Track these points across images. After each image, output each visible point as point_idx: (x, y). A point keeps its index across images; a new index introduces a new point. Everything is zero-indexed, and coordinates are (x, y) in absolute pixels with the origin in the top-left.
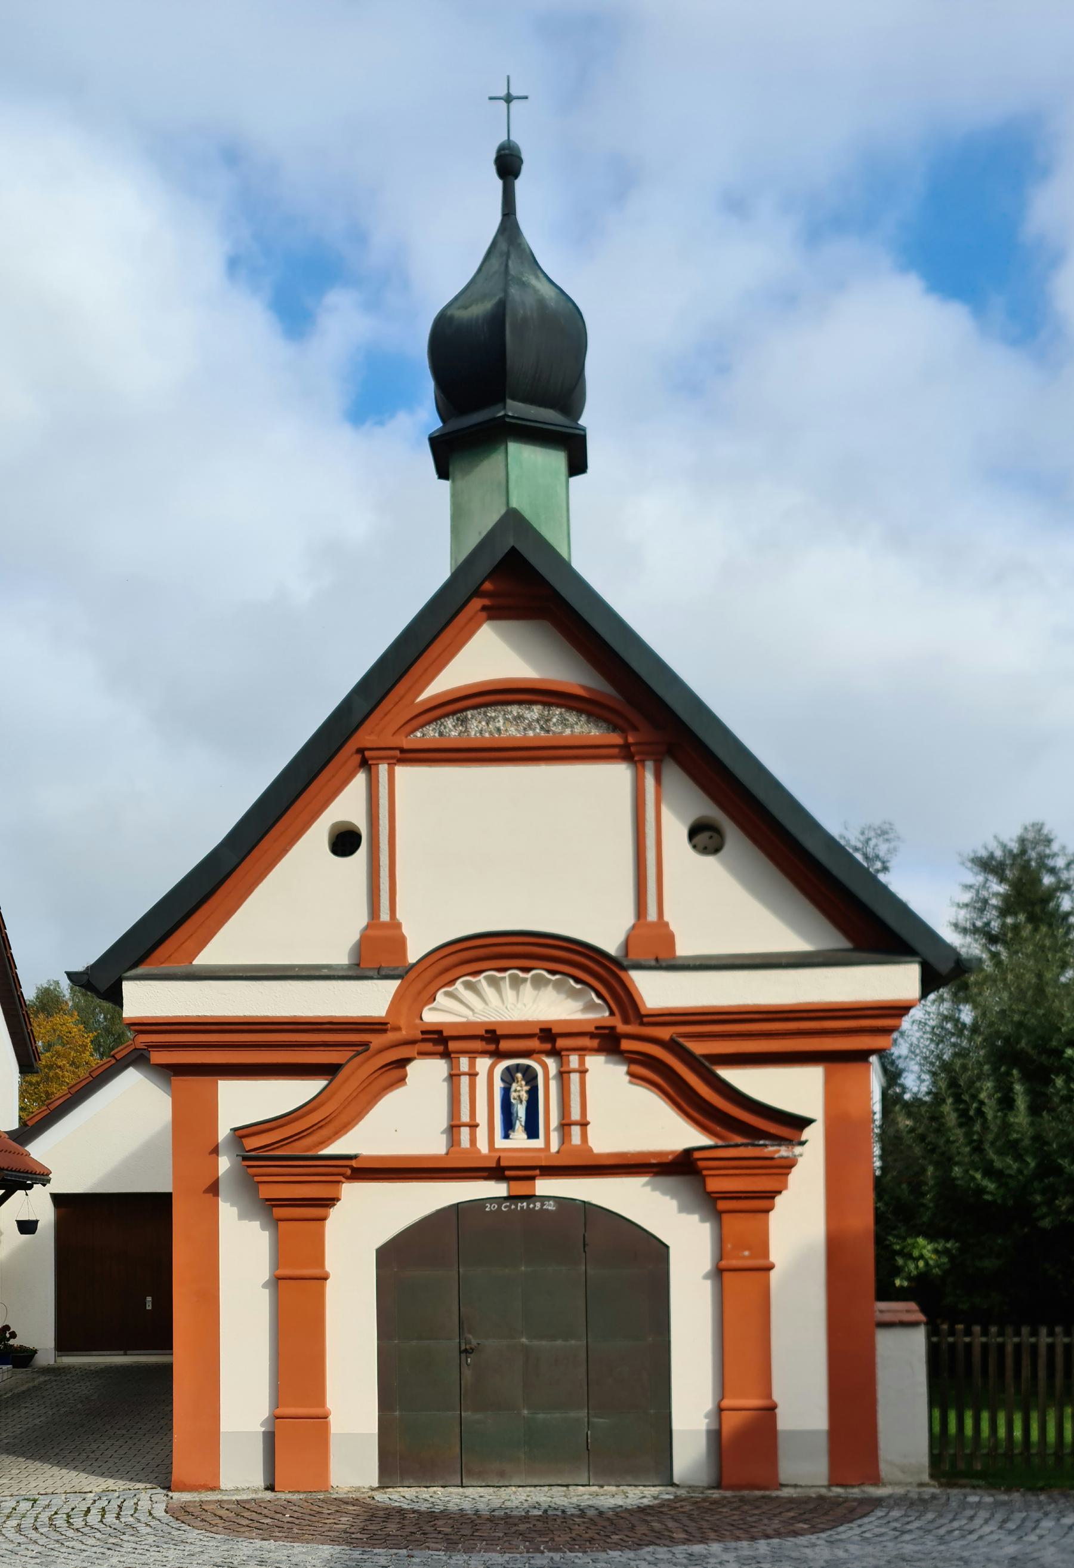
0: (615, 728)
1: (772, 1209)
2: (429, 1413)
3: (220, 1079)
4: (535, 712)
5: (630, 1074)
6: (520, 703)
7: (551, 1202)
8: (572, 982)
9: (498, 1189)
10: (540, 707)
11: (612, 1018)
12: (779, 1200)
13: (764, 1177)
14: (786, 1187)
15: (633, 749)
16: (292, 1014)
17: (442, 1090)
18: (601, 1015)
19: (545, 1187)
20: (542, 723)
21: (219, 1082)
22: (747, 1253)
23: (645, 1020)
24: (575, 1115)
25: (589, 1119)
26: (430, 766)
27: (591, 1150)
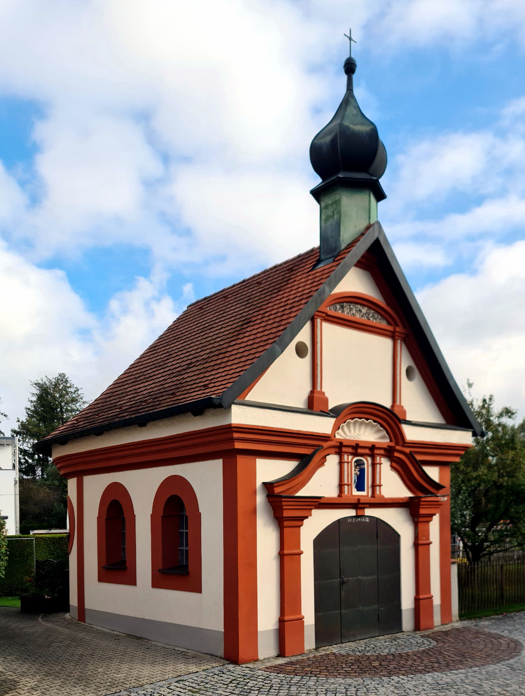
0: (389, 323)
1: (431, 521)
2: (100, 628)
3: (258, 458)
4: (365, 310)
5: (392, 466)
6: (361, 304)
7: (367, 518)
8: (379, 426)
9: (351, 513)
10: (366, 308)
11: (391, 443)
12: (305, 521)
13: (434, 509)
14: (311, 515)
15: (396, 334)
16: (299, 429)
17: (336, 468)
18: (386, 441)
19: (369, 512)
20: (367, 315)
21: (257, 459)
22: (424, 538)
23: (406, 445)
24: (378, 482)
25: (382, 483)
26: (331, 324)
27: (383, 497)
